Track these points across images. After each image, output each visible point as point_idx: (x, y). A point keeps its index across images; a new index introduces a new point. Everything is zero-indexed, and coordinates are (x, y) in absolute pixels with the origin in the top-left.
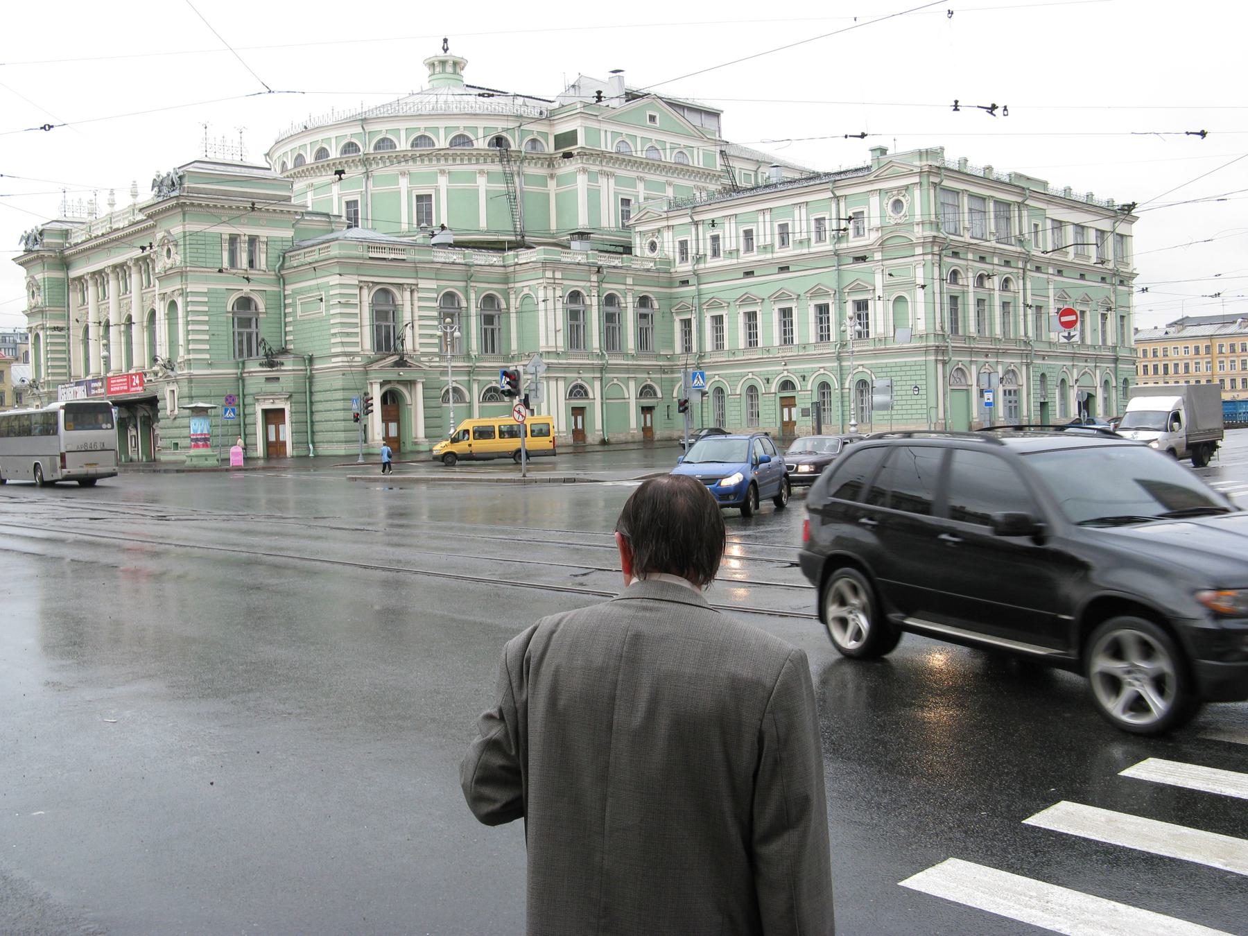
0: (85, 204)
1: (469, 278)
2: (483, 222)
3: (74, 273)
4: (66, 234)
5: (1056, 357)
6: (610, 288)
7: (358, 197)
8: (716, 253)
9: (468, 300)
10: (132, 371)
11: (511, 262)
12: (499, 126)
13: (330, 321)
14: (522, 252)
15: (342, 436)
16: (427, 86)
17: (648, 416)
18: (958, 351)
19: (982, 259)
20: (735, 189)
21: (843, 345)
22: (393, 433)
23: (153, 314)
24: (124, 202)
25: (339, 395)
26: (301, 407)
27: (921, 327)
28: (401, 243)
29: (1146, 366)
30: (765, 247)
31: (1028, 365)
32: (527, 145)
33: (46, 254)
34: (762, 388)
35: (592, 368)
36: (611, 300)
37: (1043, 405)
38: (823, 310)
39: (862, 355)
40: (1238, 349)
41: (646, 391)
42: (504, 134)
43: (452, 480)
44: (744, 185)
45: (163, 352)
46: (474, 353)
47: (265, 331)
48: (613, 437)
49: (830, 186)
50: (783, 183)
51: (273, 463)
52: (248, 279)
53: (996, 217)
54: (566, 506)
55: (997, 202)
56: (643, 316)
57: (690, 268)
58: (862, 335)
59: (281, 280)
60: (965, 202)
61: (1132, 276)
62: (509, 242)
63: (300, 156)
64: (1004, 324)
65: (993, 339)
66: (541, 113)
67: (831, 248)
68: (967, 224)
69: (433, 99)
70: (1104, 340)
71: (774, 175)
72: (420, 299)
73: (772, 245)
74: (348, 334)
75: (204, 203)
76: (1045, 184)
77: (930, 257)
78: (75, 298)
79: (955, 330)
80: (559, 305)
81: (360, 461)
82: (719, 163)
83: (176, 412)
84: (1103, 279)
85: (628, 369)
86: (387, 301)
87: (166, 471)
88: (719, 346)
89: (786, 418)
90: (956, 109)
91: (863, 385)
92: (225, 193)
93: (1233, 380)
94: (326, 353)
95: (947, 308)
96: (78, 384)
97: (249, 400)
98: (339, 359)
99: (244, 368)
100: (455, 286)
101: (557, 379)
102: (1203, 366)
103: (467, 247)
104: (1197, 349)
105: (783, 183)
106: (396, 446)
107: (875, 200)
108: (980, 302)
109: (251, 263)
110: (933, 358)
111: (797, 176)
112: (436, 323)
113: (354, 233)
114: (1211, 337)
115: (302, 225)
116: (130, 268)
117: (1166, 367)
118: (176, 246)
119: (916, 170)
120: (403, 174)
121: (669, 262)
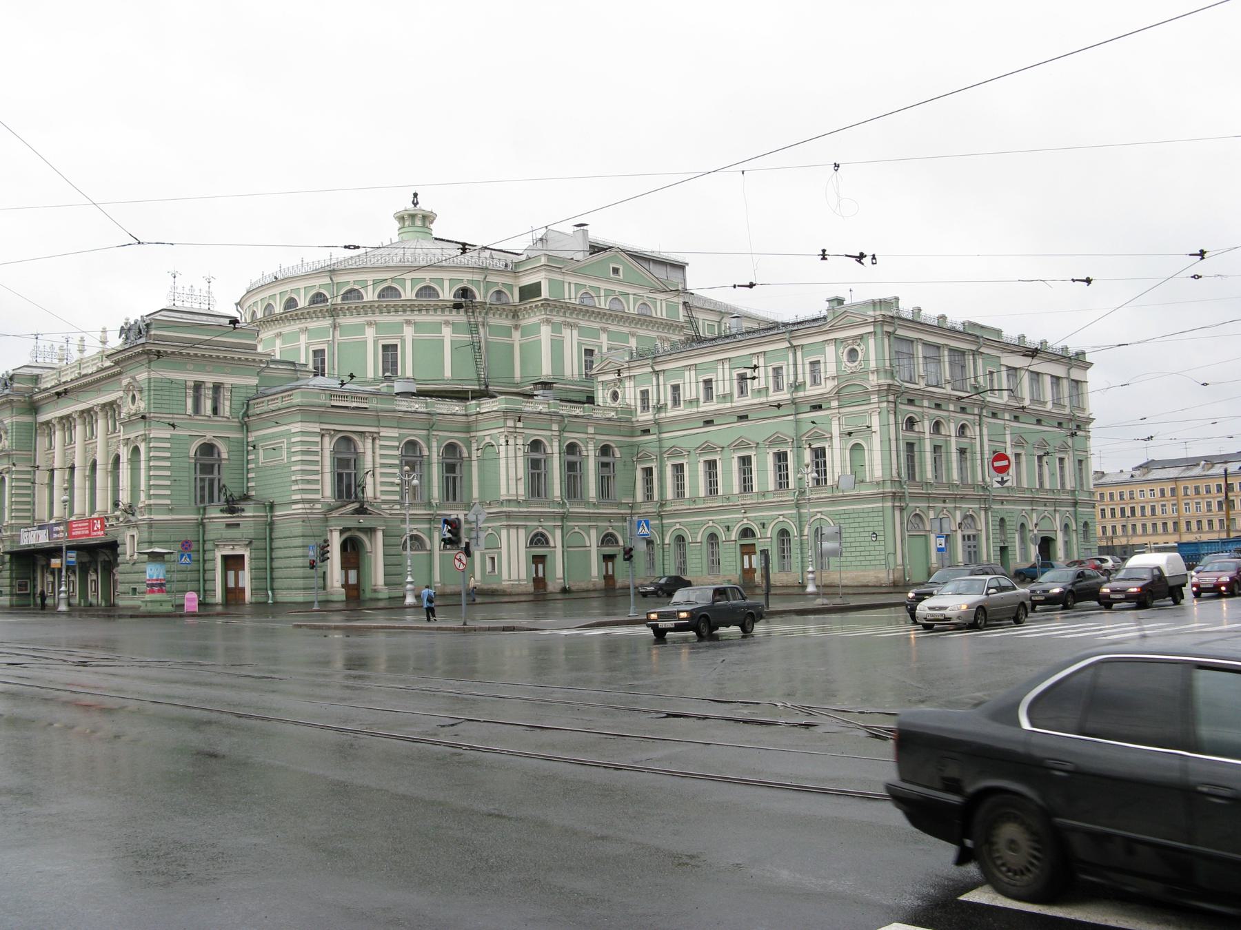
0: (57, 350)
1: (431, 427)
2: (448, 372)
3: (43, 418)
4: (36, 379)
5: (1015, 502)
6: (571, 437)
7: (325, 347)
8: (676, 402)
9: (429, 448)
10: (95, 516)
11: (473, 411)
12: (465, 279)
13: (292, 465)
14: (484, 401)
15: (301, 582)
16: (396, 239)
17: (610, 564)
18: (914, 497)
19: (938, 406)
20: (700, 340)
21: (802, 493)
22: (353, 580)
23: (117, 458)
24: (93, 349)
25: (299, 542)
26: (261, 554)
27: (878, 473)
28: (364, 392)
29: (1113, 509)
30: (724, 396)
31: (986, 510)
32: (486, 295)
33: (15, 398)
34: (722, 536)
35: (553, 516)
36: (572, 448)
37: (1003, 550)
38: (781, 457)
39: (820, 502)
40: (1203, 491)
41: (608, 539)
42: (470, 286)
43: (394, 628)
44: (709, 336)
45: (125, 498)
46: (434, 502)
47: (227, 477)
48: (574, 584)
50: (742, 334)
51: (232, 610)
52: (173, 426)
53: (951, 364)
54: (525, 652)
55: (951, 350)
57: (651, 417)
58: (820, 482)
59: (245, 426)
60: (920, 350)
61: (1089, 421)
62: (473, 391)
63: (269, 305)
64: (961, 469)
65: (951, 485)
66: (506, 266)
67: (788, 396)
68: (922, 373)
69: (402, 251)
70: (1063, 484)
71: (731, 325)
72: (382, 447)
73: (731, 395)
74: (309, 482)
75: (184, 352)
76: (999, 332)
77: (885, 405)
78: (42, 442)
79: (911, 475)
80: (520, 453)
81: (316, 608)
82: (682, 315)
83: (136, 556)
84: (1060, 424)
85: (589, 518)
86: (349, 449)
87: (121, 616)
88: (679, 493)
89: (746, 566)
90: (824, 258)
91: (818, 533)
92: (191, 341)
93: (1199, 522)
94: (285, 499)
95: (903, 455)
96: (41, 528)
97: (209, 546)
98: (300, 506)
99: (204, 514)
100: (417, 435)
101: (518, 527)
102: (1169, 508)
103: (431, 396)
104: (1162, 491)
105: (742, 334)
106: (355, 593)
107: (830, 350)
108: (936, 448)
109: (215, 410)
110: (890, 504)
111: (756, 326)
112: (397, 471)
113: (319, 381)
114: (1176, 479)
115: (267, 373)
116: (96, 413)
117: (1133, 509)
119: (870, 320)
120: (370, 324)
121: (630, 411)
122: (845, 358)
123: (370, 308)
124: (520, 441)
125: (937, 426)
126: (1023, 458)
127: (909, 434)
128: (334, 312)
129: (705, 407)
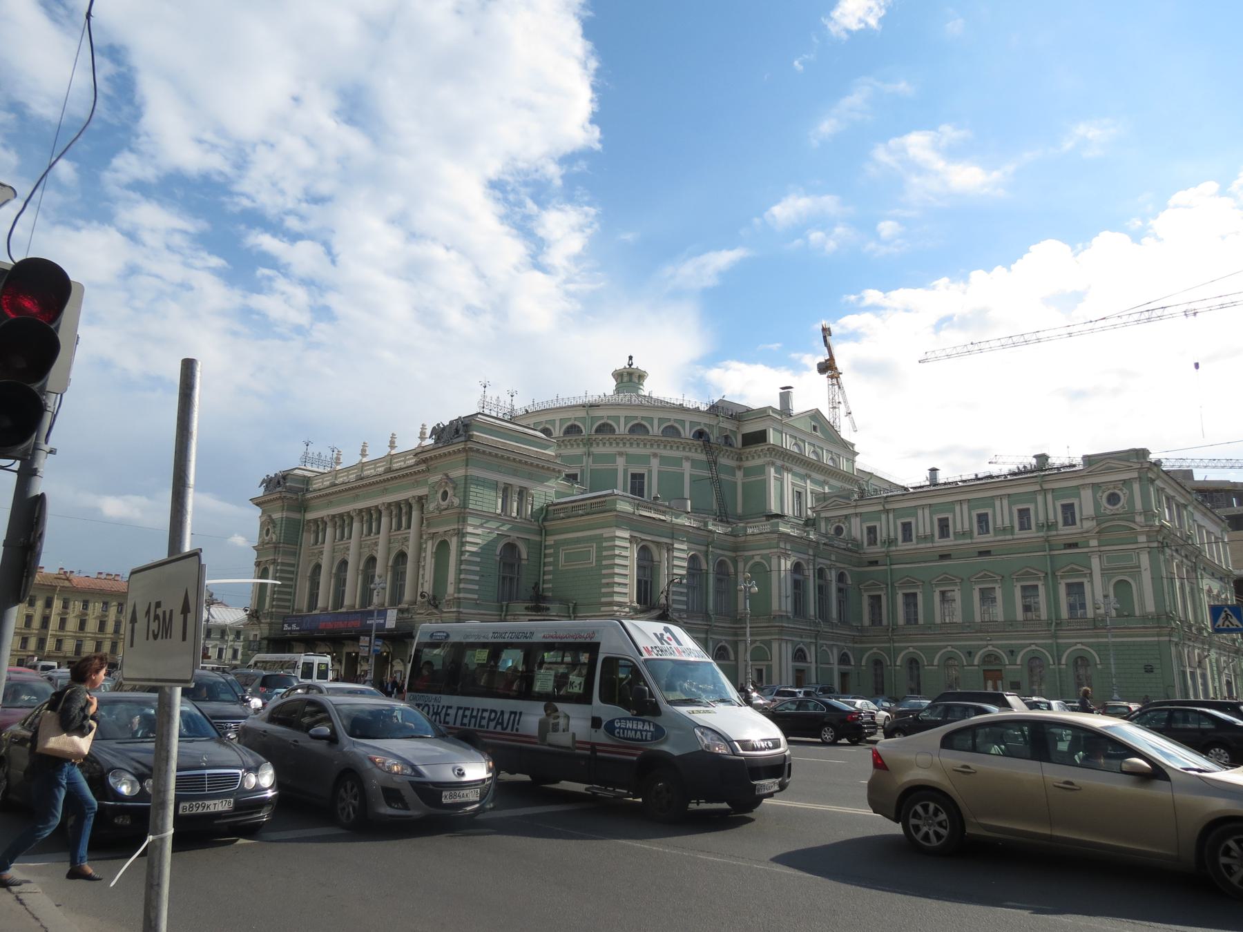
3: (310, 516)
41: (844, 659)
49: (1039, 479)
73: (971, 531)
78: (308, 538)
118: (455, 488)
121: (857, 544)
122: (1104, 501)
123: (622, 441)
128: (589, 442)
129: (940, 543)
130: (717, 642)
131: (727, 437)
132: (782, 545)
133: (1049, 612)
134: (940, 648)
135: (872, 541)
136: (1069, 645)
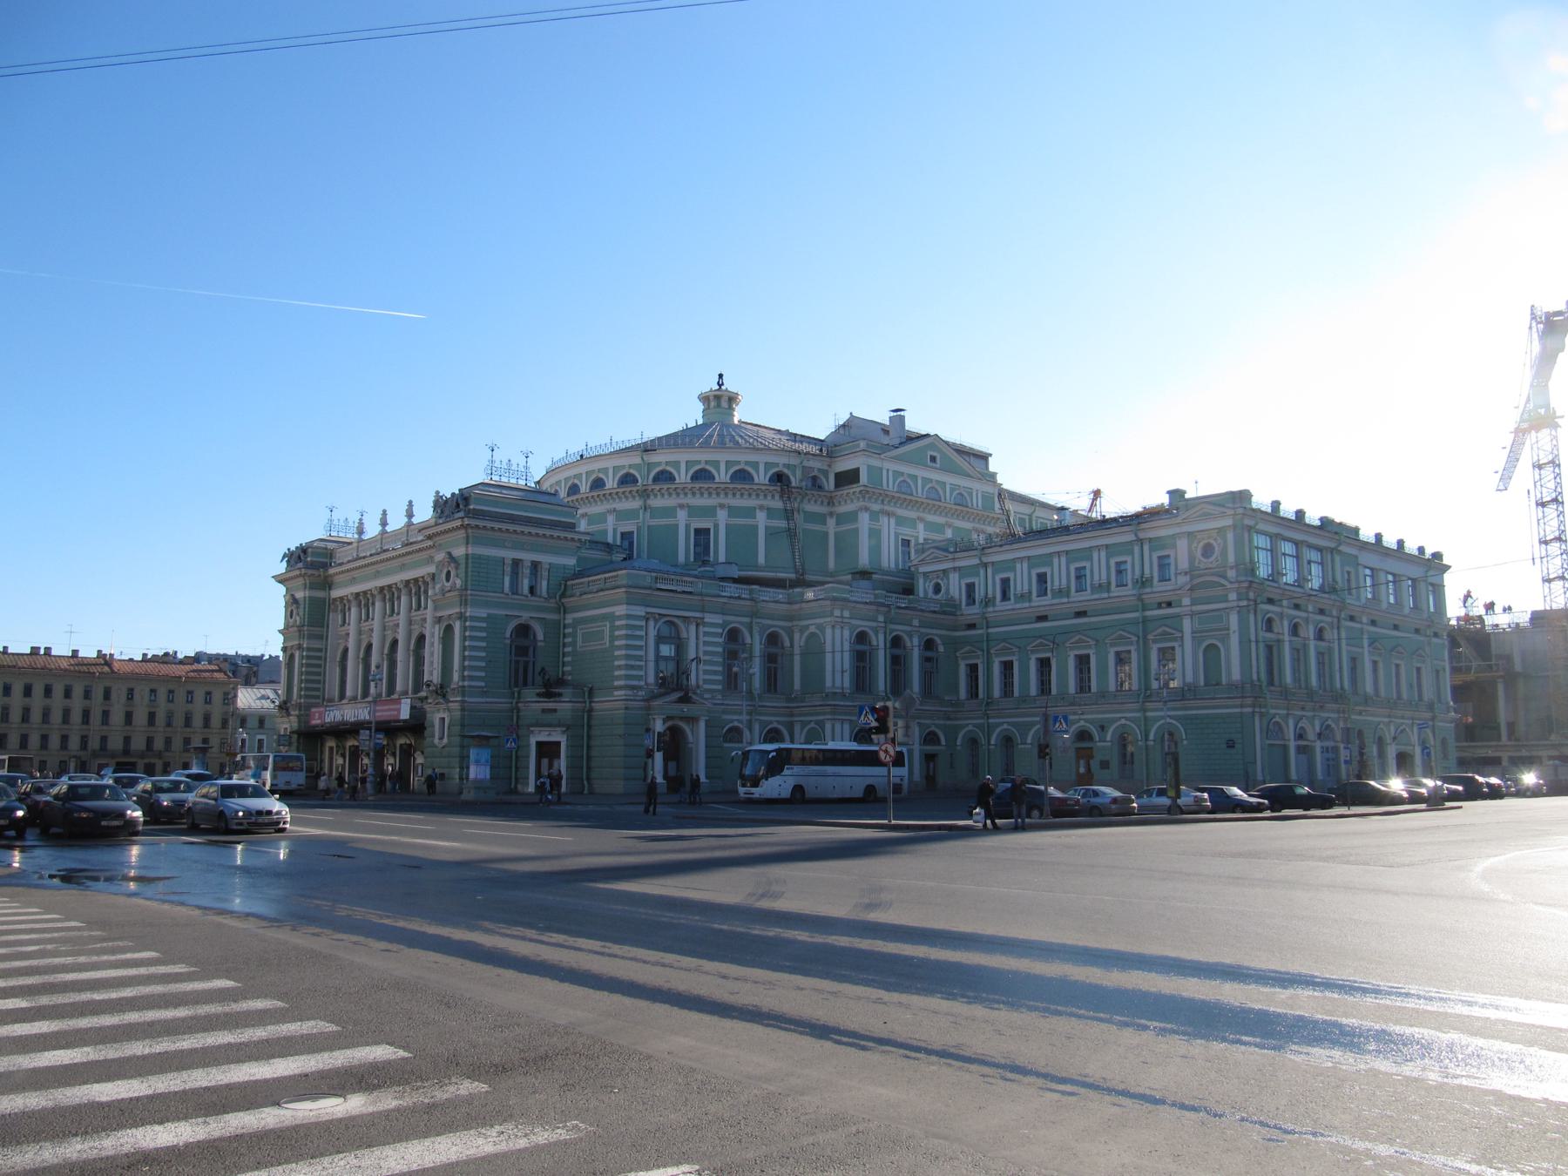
1: (754, 614)
3: (336, 594)
6: (899, 629)
24: (397, 522)
46: (756, 693)
56: (928, 659)
59: (562, 609)
70: (1420, 695)
71: (1069, 521)
72: (706, 634)
74: (632, 667)
78: (335, 618)
100: (736, 621)
116: (399, 590)
123: (683, 491)
124: (846, 633)
125: (1295, 630)
126: (1381, 665)
127: (1268, 635)
128: (645, 494)
129: (1037, 601)
130: (763, 724)
131: (814, 478)
132: (837, 613)
133: (1242, 673)
134: (998, 725)
135: (971, 599)
136: (998, 725)
